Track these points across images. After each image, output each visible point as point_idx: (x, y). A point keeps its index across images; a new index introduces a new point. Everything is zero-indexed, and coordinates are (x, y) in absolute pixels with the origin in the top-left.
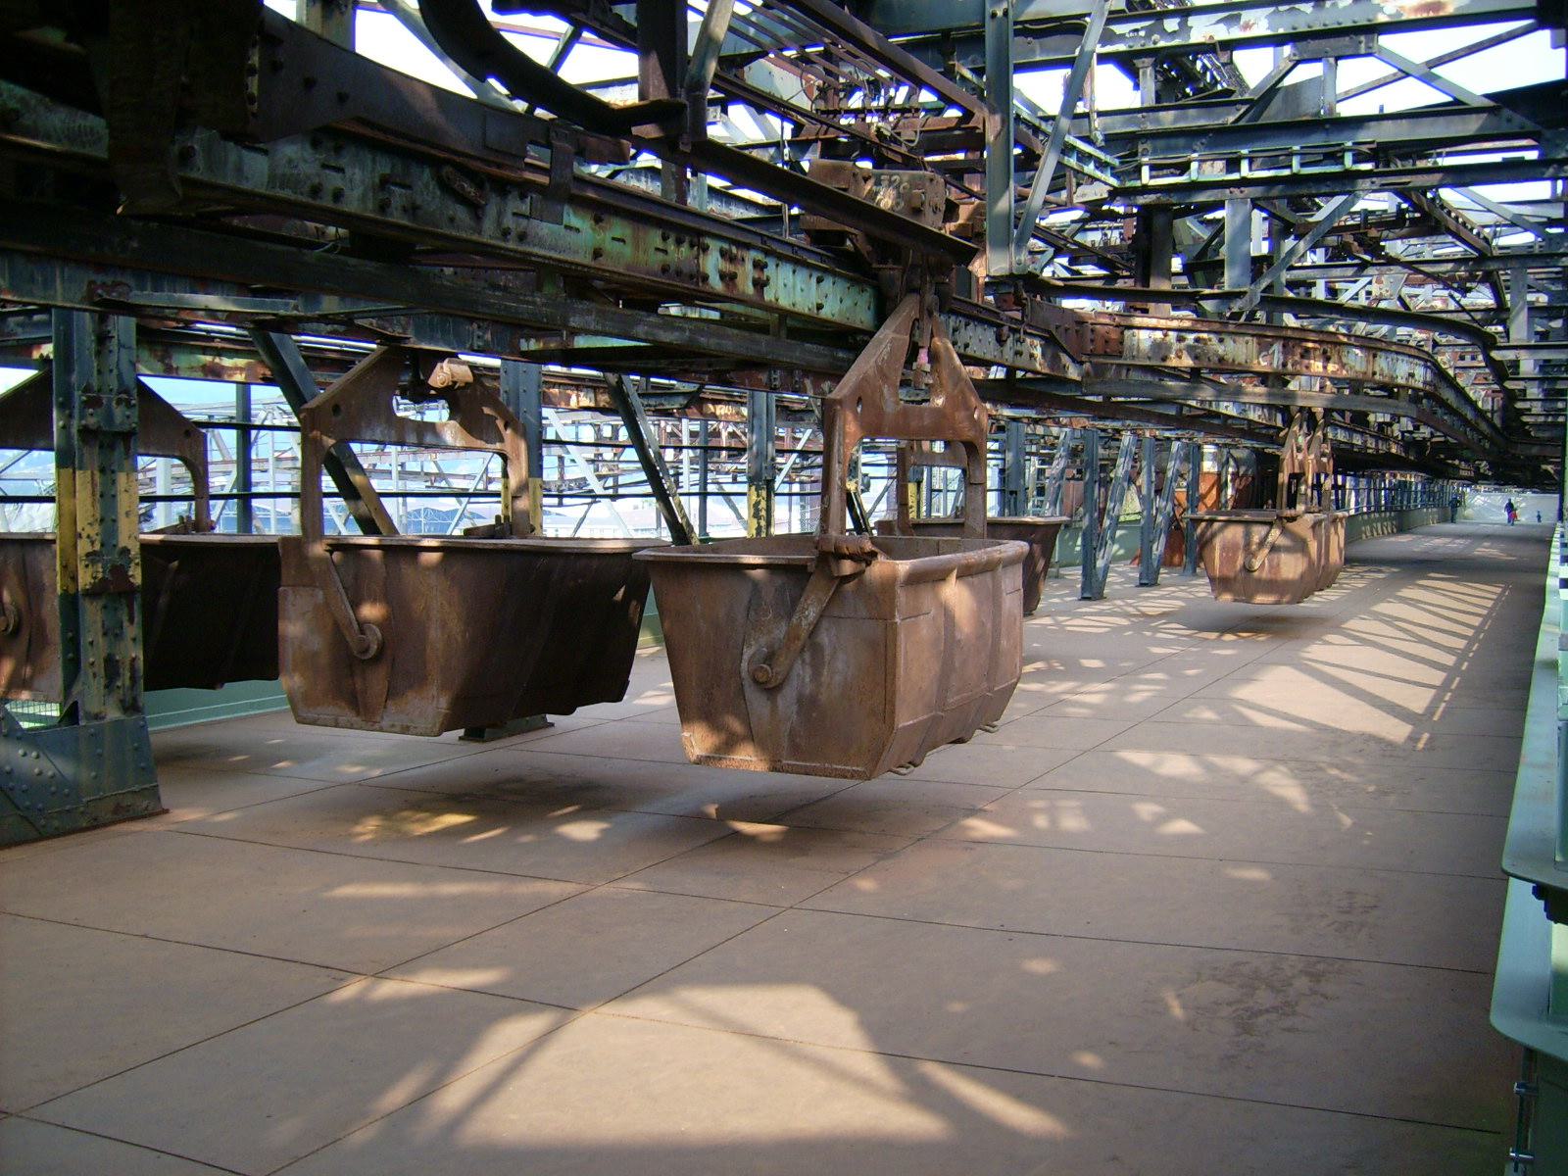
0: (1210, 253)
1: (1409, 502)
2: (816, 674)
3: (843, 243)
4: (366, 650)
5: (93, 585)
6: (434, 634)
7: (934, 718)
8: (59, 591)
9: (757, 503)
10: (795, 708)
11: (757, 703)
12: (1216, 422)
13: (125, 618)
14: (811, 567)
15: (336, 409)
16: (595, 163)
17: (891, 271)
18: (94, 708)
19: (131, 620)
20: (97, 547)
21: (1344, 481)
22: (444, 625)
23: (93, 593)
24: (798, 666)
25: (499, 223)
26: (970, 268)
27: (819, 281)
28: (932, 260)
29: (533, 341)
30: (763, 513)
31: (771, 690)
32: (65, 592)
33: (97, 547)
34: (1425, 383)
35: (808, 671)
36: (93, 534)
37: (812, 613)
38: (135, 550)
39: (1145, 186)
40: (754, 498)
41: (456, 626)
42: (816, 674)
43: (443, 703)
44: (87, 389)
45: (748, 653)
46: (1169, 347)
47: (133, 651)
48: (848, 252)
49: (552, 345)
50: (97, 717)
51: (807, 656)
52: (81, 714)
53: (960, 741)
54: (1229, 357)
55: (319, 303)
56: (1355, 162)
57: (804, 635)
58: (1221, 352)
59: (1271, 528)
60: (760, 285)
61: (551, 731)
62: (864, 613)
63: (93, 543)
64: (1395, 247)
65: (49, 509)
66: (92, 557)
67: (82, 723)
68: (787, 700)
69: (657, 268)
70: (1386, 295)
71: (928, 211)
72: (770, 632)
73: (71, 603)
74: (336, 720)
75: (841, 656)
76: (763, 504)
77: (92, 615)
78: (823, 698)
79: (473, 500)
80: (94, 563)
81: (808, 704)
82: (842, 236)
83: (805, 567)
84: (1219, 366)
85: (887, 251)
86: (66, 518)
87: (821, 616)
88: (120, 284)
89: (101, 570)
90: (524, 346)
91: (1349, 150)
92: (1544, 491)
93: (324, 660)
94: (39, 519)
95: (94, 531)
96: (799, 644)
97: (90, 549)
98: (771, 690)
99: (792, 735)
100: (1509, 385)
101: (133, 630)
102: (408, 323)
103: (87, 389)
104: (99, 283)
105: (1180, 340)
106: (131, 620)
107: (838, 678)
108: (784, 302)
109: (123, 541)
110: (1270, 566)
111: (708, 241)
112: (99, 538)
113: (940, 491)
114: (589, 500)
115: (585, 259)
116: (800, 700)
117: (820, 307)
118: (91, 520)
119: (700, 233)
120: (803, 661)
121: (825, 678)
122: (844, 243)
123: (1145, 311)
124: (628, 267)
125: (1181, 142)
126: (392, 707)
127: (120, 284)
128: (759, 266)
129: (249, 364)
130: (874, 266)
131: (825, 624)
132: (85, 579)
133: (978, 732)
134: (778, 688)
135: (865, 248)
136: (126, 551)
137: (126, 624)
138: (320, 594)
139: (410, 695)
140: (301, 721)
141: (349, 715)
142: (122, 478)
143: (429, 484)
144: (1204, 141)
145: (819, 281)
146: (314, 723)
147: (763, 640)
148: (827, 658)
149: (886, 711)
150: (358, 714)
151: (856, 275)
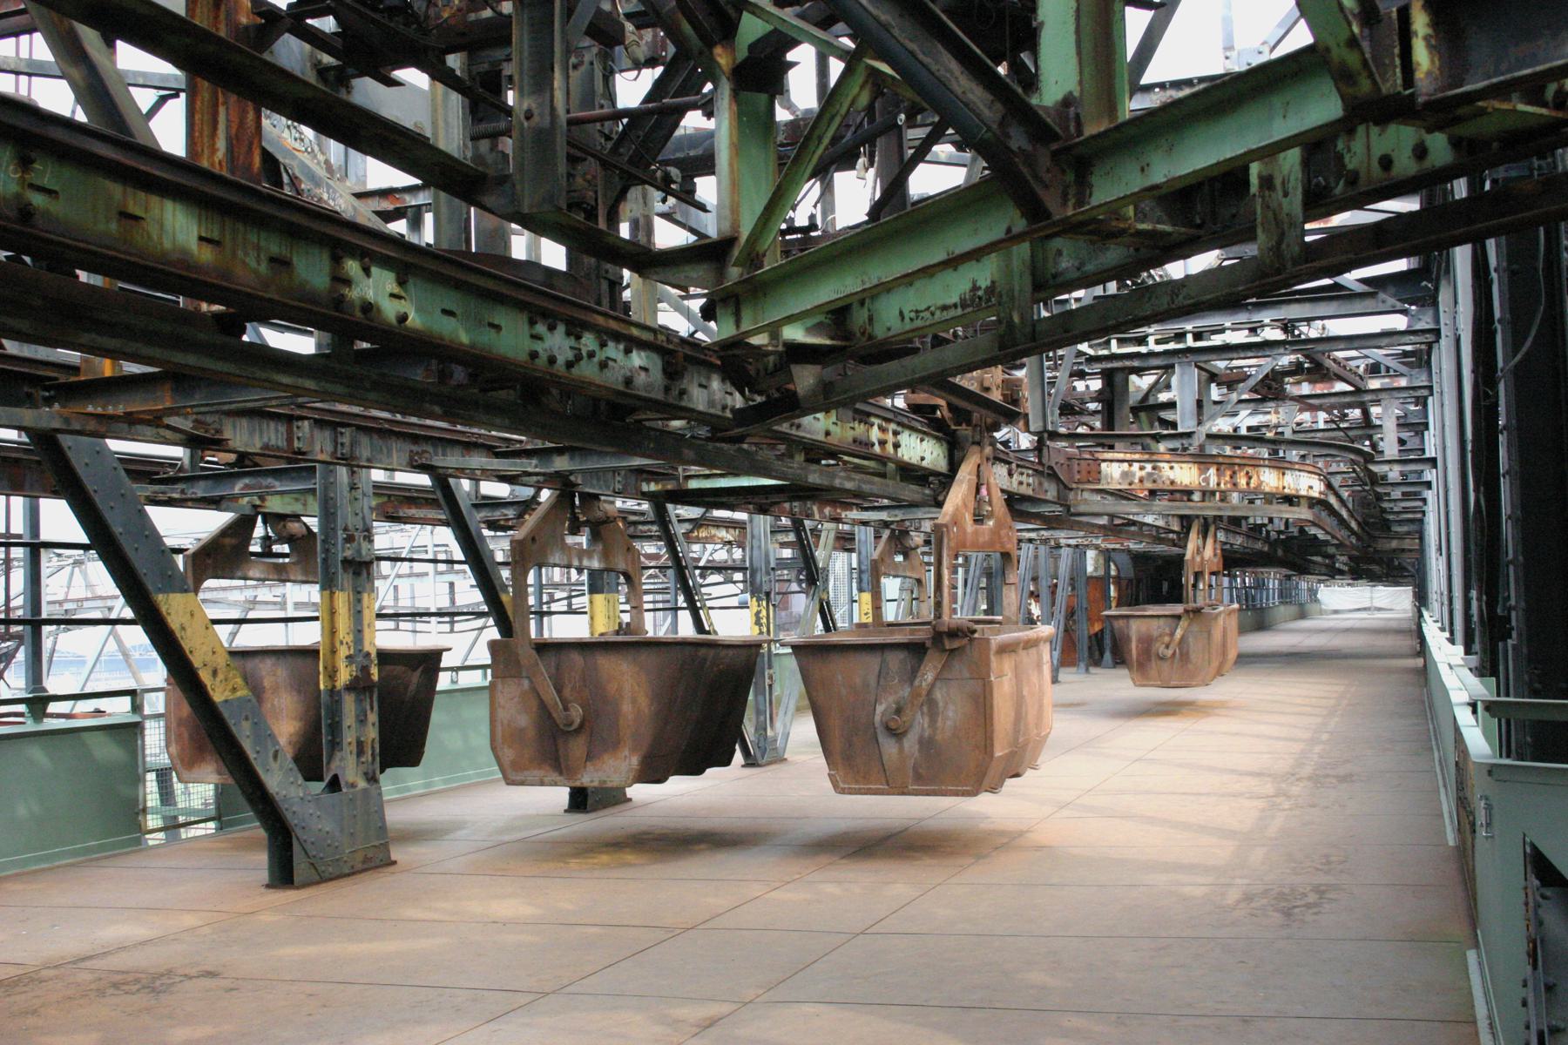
1: (1267, 599)
2: (933, 721)
3: (935, 413)
4: (571, 724)
5: (351, 681)
6: (626, 708)
7: (1011, 752)
9: (758, 613)
10: (917, 747)
11: (889, 748)
12: (1133, 528)
13: (368, 707)
14: (928, 644)
15: (533, 539)
16: (1525, 559)
17: (964, 431)
18: (351, 779)
19: (372, 708)
22: (634, 701)
23: (350, 688)
24: (919, 716)
26: (792, 366)
27: (922, 440)
28: (989, 421)
30: (764, 621)
31: (896, 734)
33: (352, 652)
34: (1320, 493)
35: (927, 719)
37: (930, 677)
38: (374, 655)
40: (755, 609)
41: (643, 702)
42: (933, 721)
43: (635, 761)
44: (345, 529)
45: (880, 709)
46: (1133, 475)
47: (372, 733)
48: (937, 419)
49: (669, 487)
50: (353, 785)
51: (925, 709)
52: (343, 784)
53: (1017, 775)
54: (1178, 481)
55: (552, 462)
57: (924, 693)
58: (1172, 477)
60: (897, 446)
61: (629, 805)
62: (968, 675)
64: (1292, 389)
65: (316, 626)
67: (344, 790)
68: (911, 742)
69: (851, 440)
70: (1283, 423)
71: (994, 389)
72: (896, 693)
75: (951, 707)
76: (764, 613)
78: (939, 737)
80: (351, 663)
81: (926, 744)
82: (934, 408)
83: (924, 644)
84: (1171, 488)
85: (961, 416)
86: (331, 631)
87: (936, 679)
88: (426, 452)
90: (645, 488)
92: (1397, 584)
93: (531, 733)
94: (308, 635)
95: (349, 639)
96: (921, 700)
98: (896, 734)
99: (915, 769)
100: (1380, 490)
101: (373, 717)
103: (345, 529)
105: (1142, 468)
106: (372, 708)
107: (949, 723)
108: (906, 458)
109: (367, 648)
110: (1181, 655)
111: (873, 419)
115: (821, 437)
116: (921, 741)
117: (923, 459)
119: (869, 415)
120: (922, 714)
121: (939, 724)
123: (1111, 447)
124: (840, 441)
126: (590, 767)
127: (426, 452)
128: (896, 433)
130: (953, 427)
131: (938, 684)
132: (344, 675)
134: (904, 734)
135: (947, 414)
136: (368, 654)
138: (526, 683)
139: (606, 757)
140: (510, 782)
141: (555, 776)
142: (365, 596)
145: (922, 440)
146: (522, 783)
147: (891, 699)
148: (941, 710)
149: (987, 746)
150: (561, 773)
151: (940, 435)
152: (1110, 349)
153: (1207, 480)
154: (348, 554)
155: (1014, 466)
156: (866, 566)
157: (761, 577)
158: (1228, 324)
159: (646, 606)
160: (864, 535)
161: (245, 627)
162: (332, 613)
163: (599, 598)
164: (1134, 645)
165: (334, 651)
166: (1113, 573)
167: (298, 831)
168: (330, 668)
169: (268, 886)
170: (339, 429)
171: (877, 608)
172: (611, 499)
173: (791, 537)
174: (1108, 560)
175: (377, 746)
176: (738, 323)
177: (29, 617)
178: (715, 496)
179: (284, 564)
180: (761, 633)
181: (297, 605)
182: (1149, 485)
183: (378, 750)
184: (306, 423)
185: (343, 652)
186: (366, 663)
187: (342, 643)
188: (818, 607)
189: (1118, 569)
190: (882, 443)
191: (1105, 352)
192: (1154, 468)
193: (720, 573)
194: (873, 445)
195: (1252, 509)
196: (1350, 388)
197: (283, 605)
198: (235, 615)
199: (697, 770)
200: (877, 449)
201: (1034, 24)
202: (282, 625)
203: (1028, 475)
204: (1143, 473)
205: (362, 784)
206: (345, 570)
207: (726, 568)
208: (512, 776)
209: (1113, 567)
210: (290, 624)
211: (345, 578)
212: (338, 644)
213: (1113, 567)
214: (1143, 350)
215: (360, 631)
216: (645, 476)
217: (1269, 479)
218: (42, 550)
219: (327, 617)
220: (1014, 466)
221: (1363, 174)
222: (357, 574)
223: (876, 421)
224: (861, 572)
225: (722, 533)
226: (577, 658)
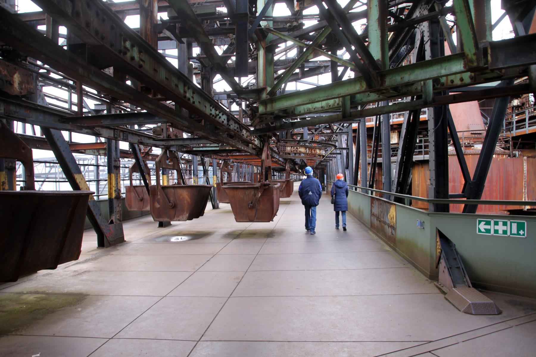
41: (189, 200)
67: (115, 223)
76: (196, 180)
90: (182, 150)
153: (307, 151)
154: (115, 164)
158: (307, 117)
159: (121, 179)
161: (45, 183)
166: (259, 172)
167: (105, 233)
170: (124, 133)
176: (266, 108)
177: (24, 180)
181: (60, 178)
182: (295, 152)
184: (118, 130)
192: (296, 148)
195: (295, 157)
196: (311, 133)
197: (56, 178)
198: (43, 180)
201: (279, 45)
202: (55, 183)
204: (294, 149)
206: (114, 169)
210: (60, 183)
212: (112, 187)
215: (117, 184)
217: (318, 151)
218: (34, 163)
221: (445, 84)
222: (117, 169)
226: (172, 190)
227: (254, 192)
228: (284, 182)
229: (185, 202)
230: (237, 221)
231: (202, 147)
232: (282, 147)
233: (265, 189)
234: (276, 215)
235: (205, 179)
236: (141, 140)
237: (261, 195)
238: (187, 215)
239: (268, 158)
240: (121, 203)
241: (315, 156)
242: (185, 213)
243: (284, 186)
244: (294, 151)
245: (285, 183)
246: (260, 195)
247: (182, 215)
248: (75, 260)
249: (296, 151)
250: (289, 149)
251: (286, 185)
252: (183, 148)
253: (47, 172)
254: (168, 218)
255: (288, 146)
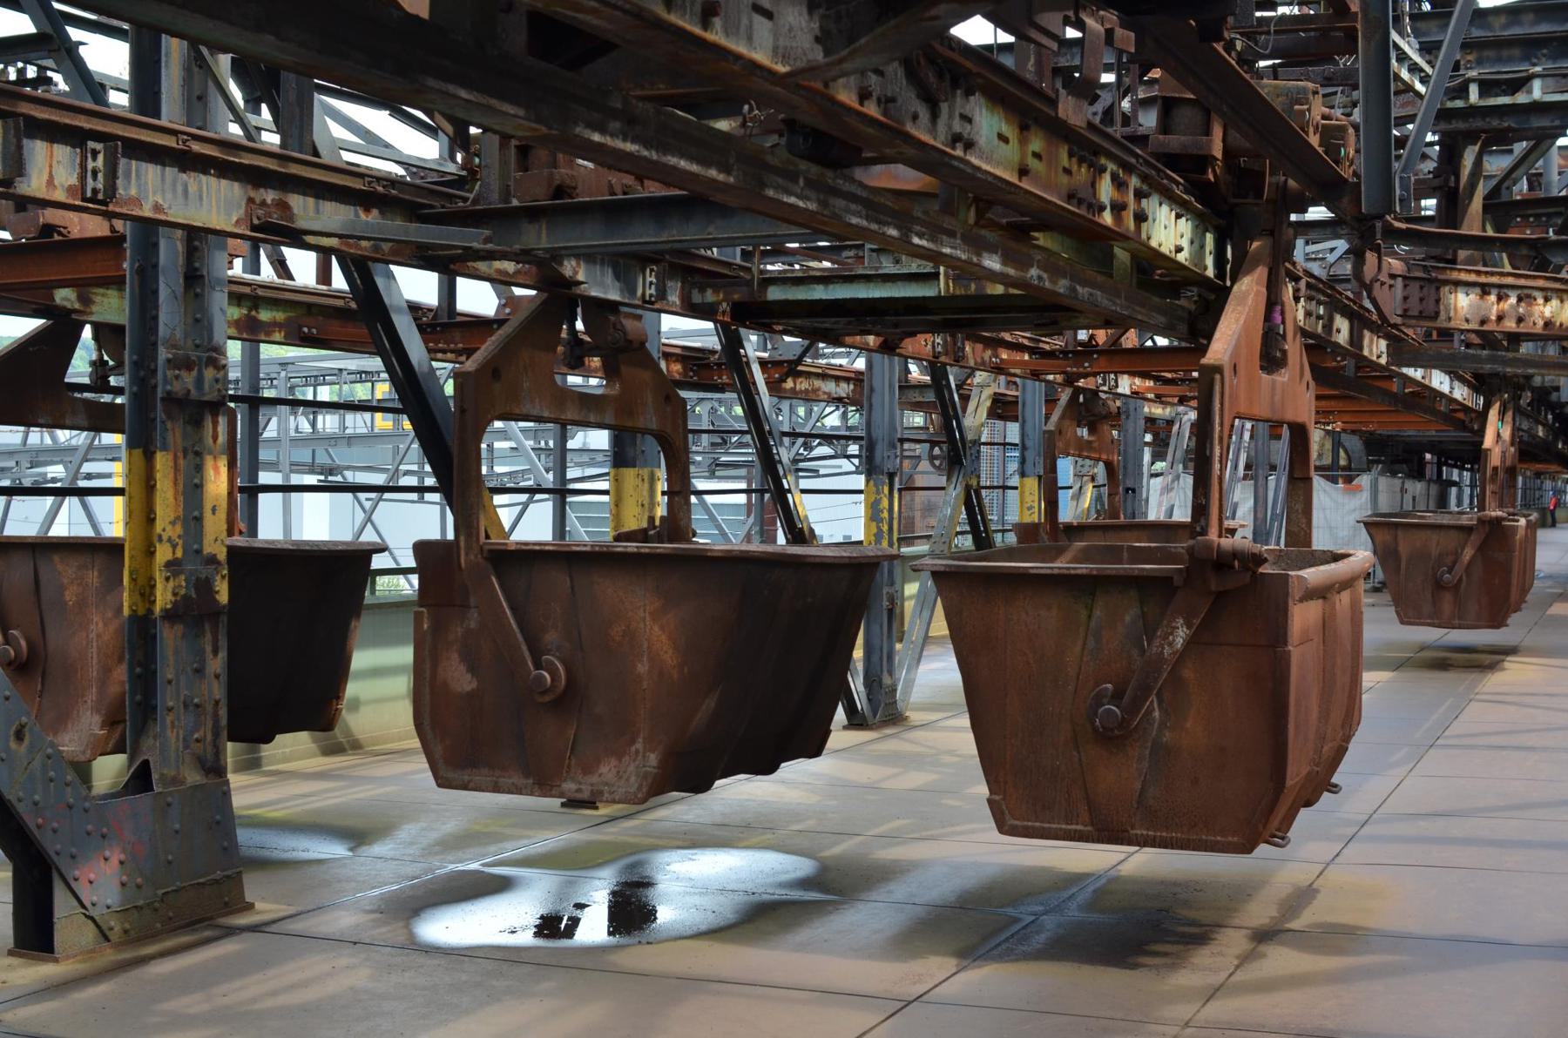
0: (1504, 192)
5: (175, 604)
8: (126, 611)
13: (209, 648)
14: (1178, 581)
19: (215, 652)
20: (179, 554)
21: (1460, 476)
23: (170, 616)
25: (950, 127)
27: (1178, 216)
29: (709, 292)
30: (886, 514)
32: (134, 616)
36: (175, 537)
38: (222, 555)
39: (1473, 108)
41: (669, 657)
50: (175, 781)
52: (155, 777)
56: (1482, 95)
59: (1470, 535)
60: (1141, 218)
63: (174, 547)
66: (173, 566)
73: (142, 630)
74: (496, 783)
76: (885, 503)
77: (169, 638)
79: (387, 495)
80: (176, 574)
89: (184, 584)
91: (1473, 80)
97: (169, 556)
101: (217, 664)
102: (578, 264)
104: (258, 201)
112: (180, 542)
113: (1016, 488)
114: (524, 497)
118: (172, 518)
122: (1205, 172)
125: (1516, 52)
128: (1139, 195)
129: (288, 319)
132: (163, 597)
133: (1325, 794)
136: (212, 560)
137: (209, 655)
143: (322, 478)
144: (1545, 51)
145: (1178, 216)
152: (1467, 98)
155: (1302, 284)
156: (1034, 441)
157: (881, 451)
160: (1032, 395)
162: (150, 487)
163: (629, 474)
164: (650, 400)
165: (150, 553)
166: (1343, 462)
168: (141, 581)
169: (11, 953)
170: (91, 144)
171: (1052, 505)
172: (639, 312)
173: (930, 397)
174: (1337, 445)
175: (223, 712)
178: (809, 315)
179: (112, 405)
180: (878, 536)
183: (224, 722)
185: (163, 554)
186: (204, 572)
187: (160, 539)
188: (962, 496)
189: (1349, 458)
190: (1118, 208)
191: (1459, 104)
193: (830, 444)
194: (1102, 208)
199: (766, 766)
200: (1107, 218)
202: (279, 495)
203: (1319, 303)
205: (193, 777)
207: (838, 438)
208: (450, 774)
209: (1342, 453)
210: (294, 495)
211: (175, 432)
213: (1342, 453)
214: (1521, 98)
216: (697, 278)
219: (138, 492)
220: (1302, 284)
223: (1111, 166)
224: (1024, 448)
225: (829, 387)
226: (559, 580)
227: (1144, 615)
228: (1467, 530)
229: (642, 668)
230: (1003, 828)
231: (826, 279)
232: (1414, 287)
233: (1220, 596)
234: (1334, 789)
235: (955, 493)
236: (284, 206)
237: (1190, 643)
238: (653, 759)
239: (1271, 359)
240: (223, 655)
241: (1326, 79)
242: (639, 745)
243: (1468, 553)
244: (1500, 318)
245: (1475, 539)
246: (1181, 636)
247: (620, 757)
248: (810, 757)
249: (1520, 320)
250: (1463, 303)
251: (1481, 549)
252: (702, 290)
253: (68, 437)
254: (527, 776)
255: (1458, 284)
